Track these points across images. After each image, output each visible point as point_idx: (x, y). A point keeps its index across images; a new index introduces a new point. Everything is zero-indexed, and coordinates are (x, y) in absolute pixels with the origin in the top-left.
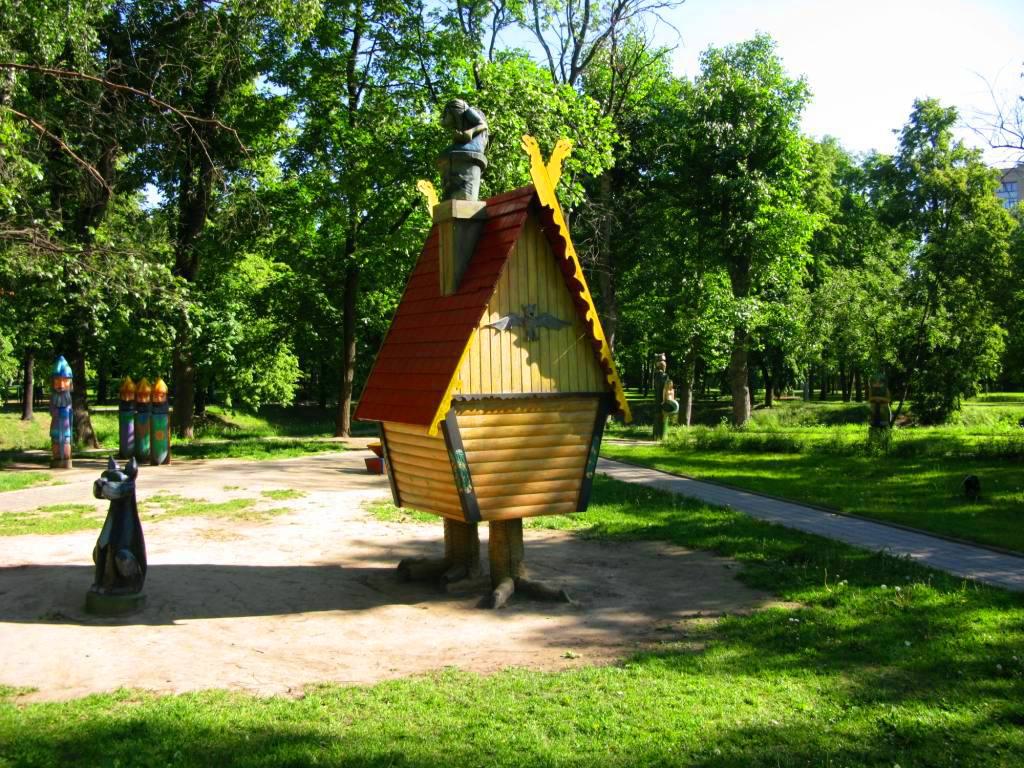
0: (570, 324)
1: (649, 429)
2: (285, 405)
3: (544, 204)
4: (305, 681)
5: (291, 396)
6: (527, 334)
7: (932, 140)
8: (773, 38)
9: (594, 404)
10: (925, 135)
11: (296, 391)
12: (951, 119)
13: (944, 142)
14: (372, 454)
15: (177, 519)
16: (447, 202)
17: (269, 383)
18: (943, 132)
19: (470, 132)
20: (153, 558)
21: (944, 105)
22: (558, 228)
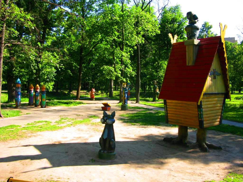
0: (221, 75)
1: (151, 99)
2: (50, 91)
3: (222, 42)
4: (212, 179)
5: (52, 89)
6: (214, 77)
7: (206, 32)
8: (181, 5)
9: (223, 96)
10: (205, 31)
11: (53, 88)
12: (211, 27)
13: (209, 32)
14: (103, 106)
15: (134, 128)
16: (191, 40)
17: (47, 86)
18: (209, 30)
19: (196, 21)
20: (116, 140)
21: (210, 24)
22: (224, 48)
